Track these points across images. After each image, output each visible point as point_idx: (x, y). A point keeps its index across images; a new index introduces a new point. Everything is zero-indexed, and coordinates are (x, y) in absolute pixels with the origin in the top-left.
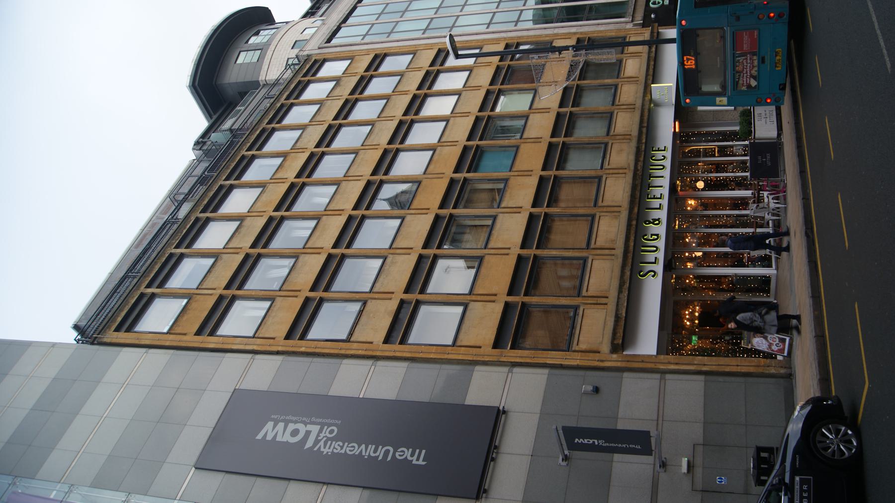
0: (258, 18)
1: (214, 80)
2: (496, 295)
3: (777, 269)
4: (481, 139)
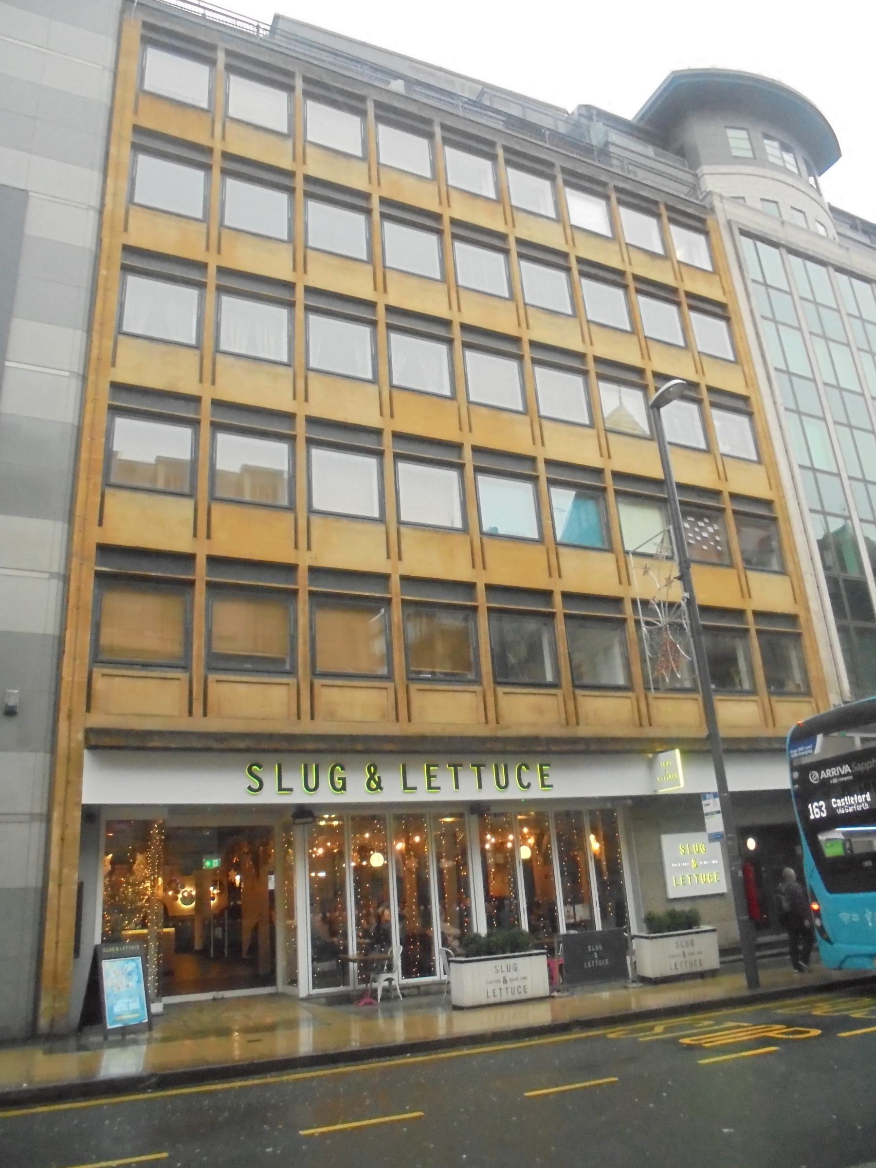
0: (811, 139)
1: (692, 106)
2: (209, 537)
3: (309, 999)
4: (735, 512)
